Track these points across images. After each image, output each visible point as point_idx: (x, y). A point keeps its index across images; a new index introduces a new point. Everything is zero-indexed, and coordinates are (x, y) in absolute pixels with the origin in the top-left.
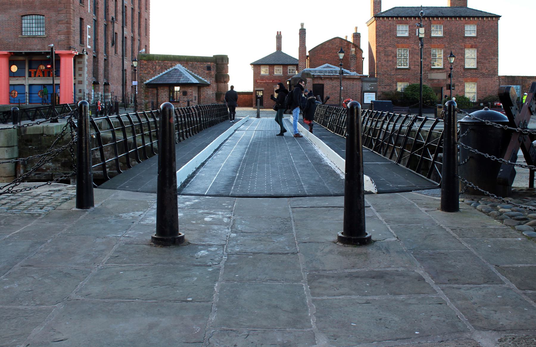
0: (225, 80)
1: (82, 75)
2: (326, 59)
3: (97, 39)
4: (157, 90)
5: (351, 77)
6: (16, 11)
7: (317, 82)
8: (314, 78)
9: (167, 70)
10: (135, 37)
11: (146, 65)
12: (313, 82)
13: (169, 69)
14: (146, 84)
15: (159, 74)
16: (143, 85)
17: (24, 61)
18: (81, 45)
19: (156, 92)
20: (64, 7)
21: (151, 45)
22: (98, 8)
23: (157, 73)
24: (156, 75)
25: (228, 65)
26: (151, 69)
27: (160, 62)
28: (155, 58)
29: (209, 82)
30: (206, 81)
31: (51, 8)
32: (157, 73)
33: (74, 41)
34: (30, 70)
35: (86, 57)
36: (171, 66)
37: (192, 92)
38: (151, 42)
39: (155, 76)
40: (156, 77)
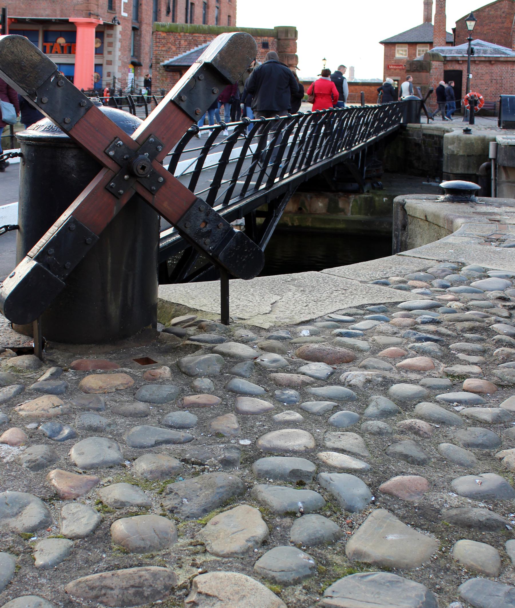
1: (113, 53)
2: (485, 32)
3: (141, 4)
5: (509, 59)
7: (450, 67)
8: (446, 61)
9: (197, 46)
10: (210, 4)
11: (164, 38)
12: (444, 67)
13: (201, 45)
14: (164, 66)
15: (185, 52)
17: (37, 31)
18: (109, 11)
21: (238, 16)
25: (297, 41)
27: (187, 34)
28: (179, 29)
33: (98, 5)
34: (45, 44)
35: (119, 28)
38: (238, 11)
39: (179, 55)
40: (180, 56)
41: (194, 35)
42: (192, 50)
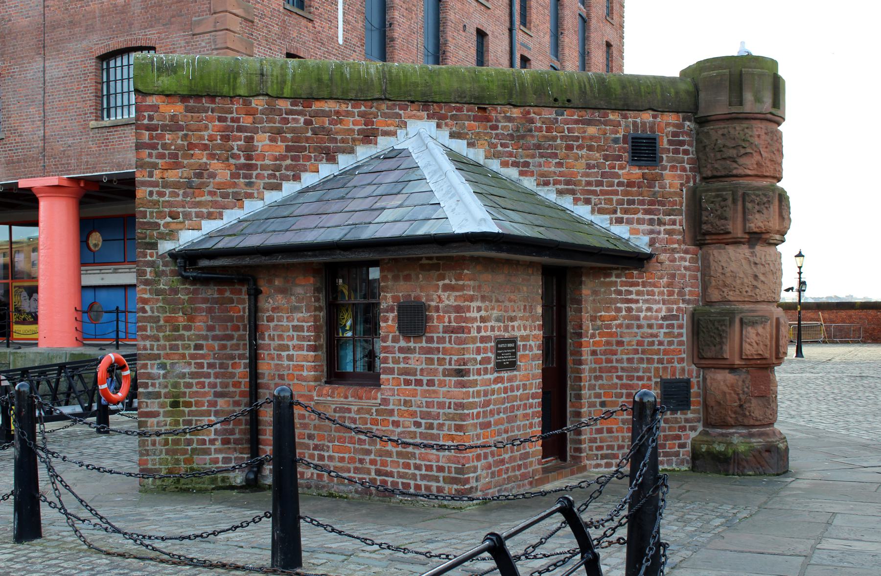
0: (757, 222)
4: (255, 294)
6: (84, 43)
9: (332, 159)
11: (174, 126)
13: (351, 151)
15: (278, 187)
16: (152, 264)
19: (242, 309)
20: (210, 10)
22: (393, 40)
23: (261, 183)
24: (250, 196)
26: (212, 156)
29: (646, 239)
30: (621, 231)
31: (173, 19)
32: (261, 183)
36: (369, 137)
37: (458, 309)
39: (247, 203)
40: (252, 207)
41: (316, 106)
42: (308, 179)
